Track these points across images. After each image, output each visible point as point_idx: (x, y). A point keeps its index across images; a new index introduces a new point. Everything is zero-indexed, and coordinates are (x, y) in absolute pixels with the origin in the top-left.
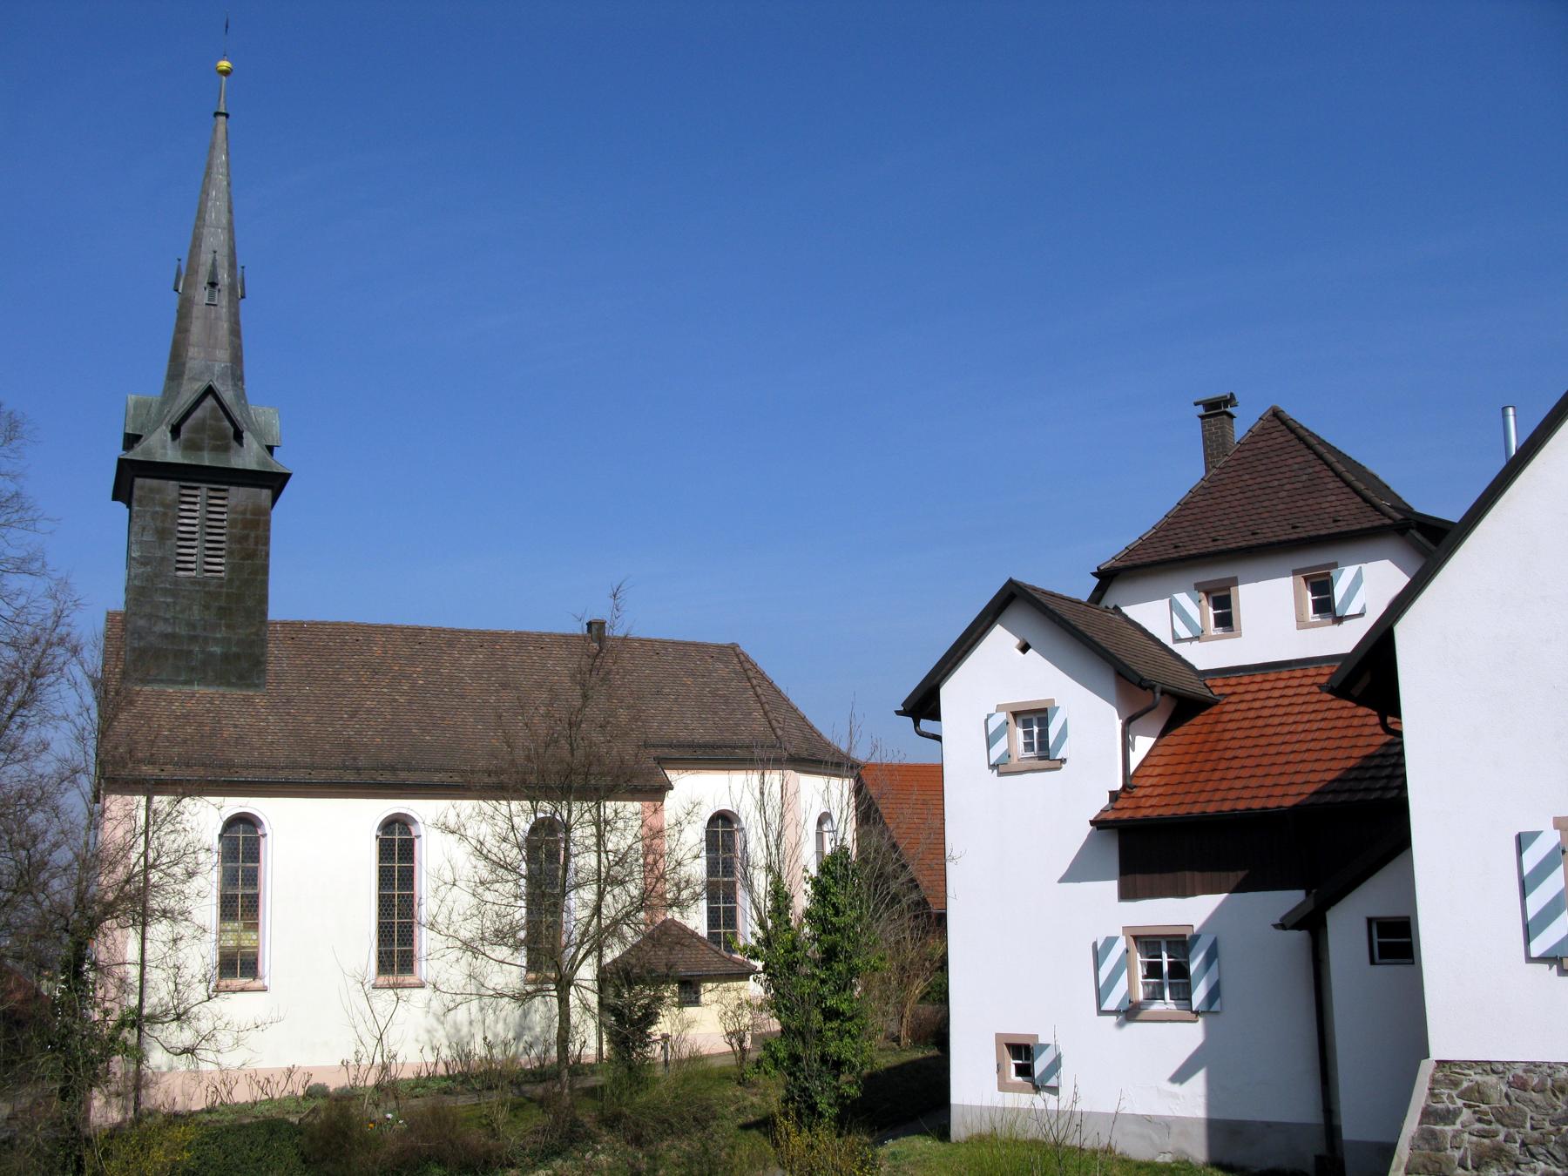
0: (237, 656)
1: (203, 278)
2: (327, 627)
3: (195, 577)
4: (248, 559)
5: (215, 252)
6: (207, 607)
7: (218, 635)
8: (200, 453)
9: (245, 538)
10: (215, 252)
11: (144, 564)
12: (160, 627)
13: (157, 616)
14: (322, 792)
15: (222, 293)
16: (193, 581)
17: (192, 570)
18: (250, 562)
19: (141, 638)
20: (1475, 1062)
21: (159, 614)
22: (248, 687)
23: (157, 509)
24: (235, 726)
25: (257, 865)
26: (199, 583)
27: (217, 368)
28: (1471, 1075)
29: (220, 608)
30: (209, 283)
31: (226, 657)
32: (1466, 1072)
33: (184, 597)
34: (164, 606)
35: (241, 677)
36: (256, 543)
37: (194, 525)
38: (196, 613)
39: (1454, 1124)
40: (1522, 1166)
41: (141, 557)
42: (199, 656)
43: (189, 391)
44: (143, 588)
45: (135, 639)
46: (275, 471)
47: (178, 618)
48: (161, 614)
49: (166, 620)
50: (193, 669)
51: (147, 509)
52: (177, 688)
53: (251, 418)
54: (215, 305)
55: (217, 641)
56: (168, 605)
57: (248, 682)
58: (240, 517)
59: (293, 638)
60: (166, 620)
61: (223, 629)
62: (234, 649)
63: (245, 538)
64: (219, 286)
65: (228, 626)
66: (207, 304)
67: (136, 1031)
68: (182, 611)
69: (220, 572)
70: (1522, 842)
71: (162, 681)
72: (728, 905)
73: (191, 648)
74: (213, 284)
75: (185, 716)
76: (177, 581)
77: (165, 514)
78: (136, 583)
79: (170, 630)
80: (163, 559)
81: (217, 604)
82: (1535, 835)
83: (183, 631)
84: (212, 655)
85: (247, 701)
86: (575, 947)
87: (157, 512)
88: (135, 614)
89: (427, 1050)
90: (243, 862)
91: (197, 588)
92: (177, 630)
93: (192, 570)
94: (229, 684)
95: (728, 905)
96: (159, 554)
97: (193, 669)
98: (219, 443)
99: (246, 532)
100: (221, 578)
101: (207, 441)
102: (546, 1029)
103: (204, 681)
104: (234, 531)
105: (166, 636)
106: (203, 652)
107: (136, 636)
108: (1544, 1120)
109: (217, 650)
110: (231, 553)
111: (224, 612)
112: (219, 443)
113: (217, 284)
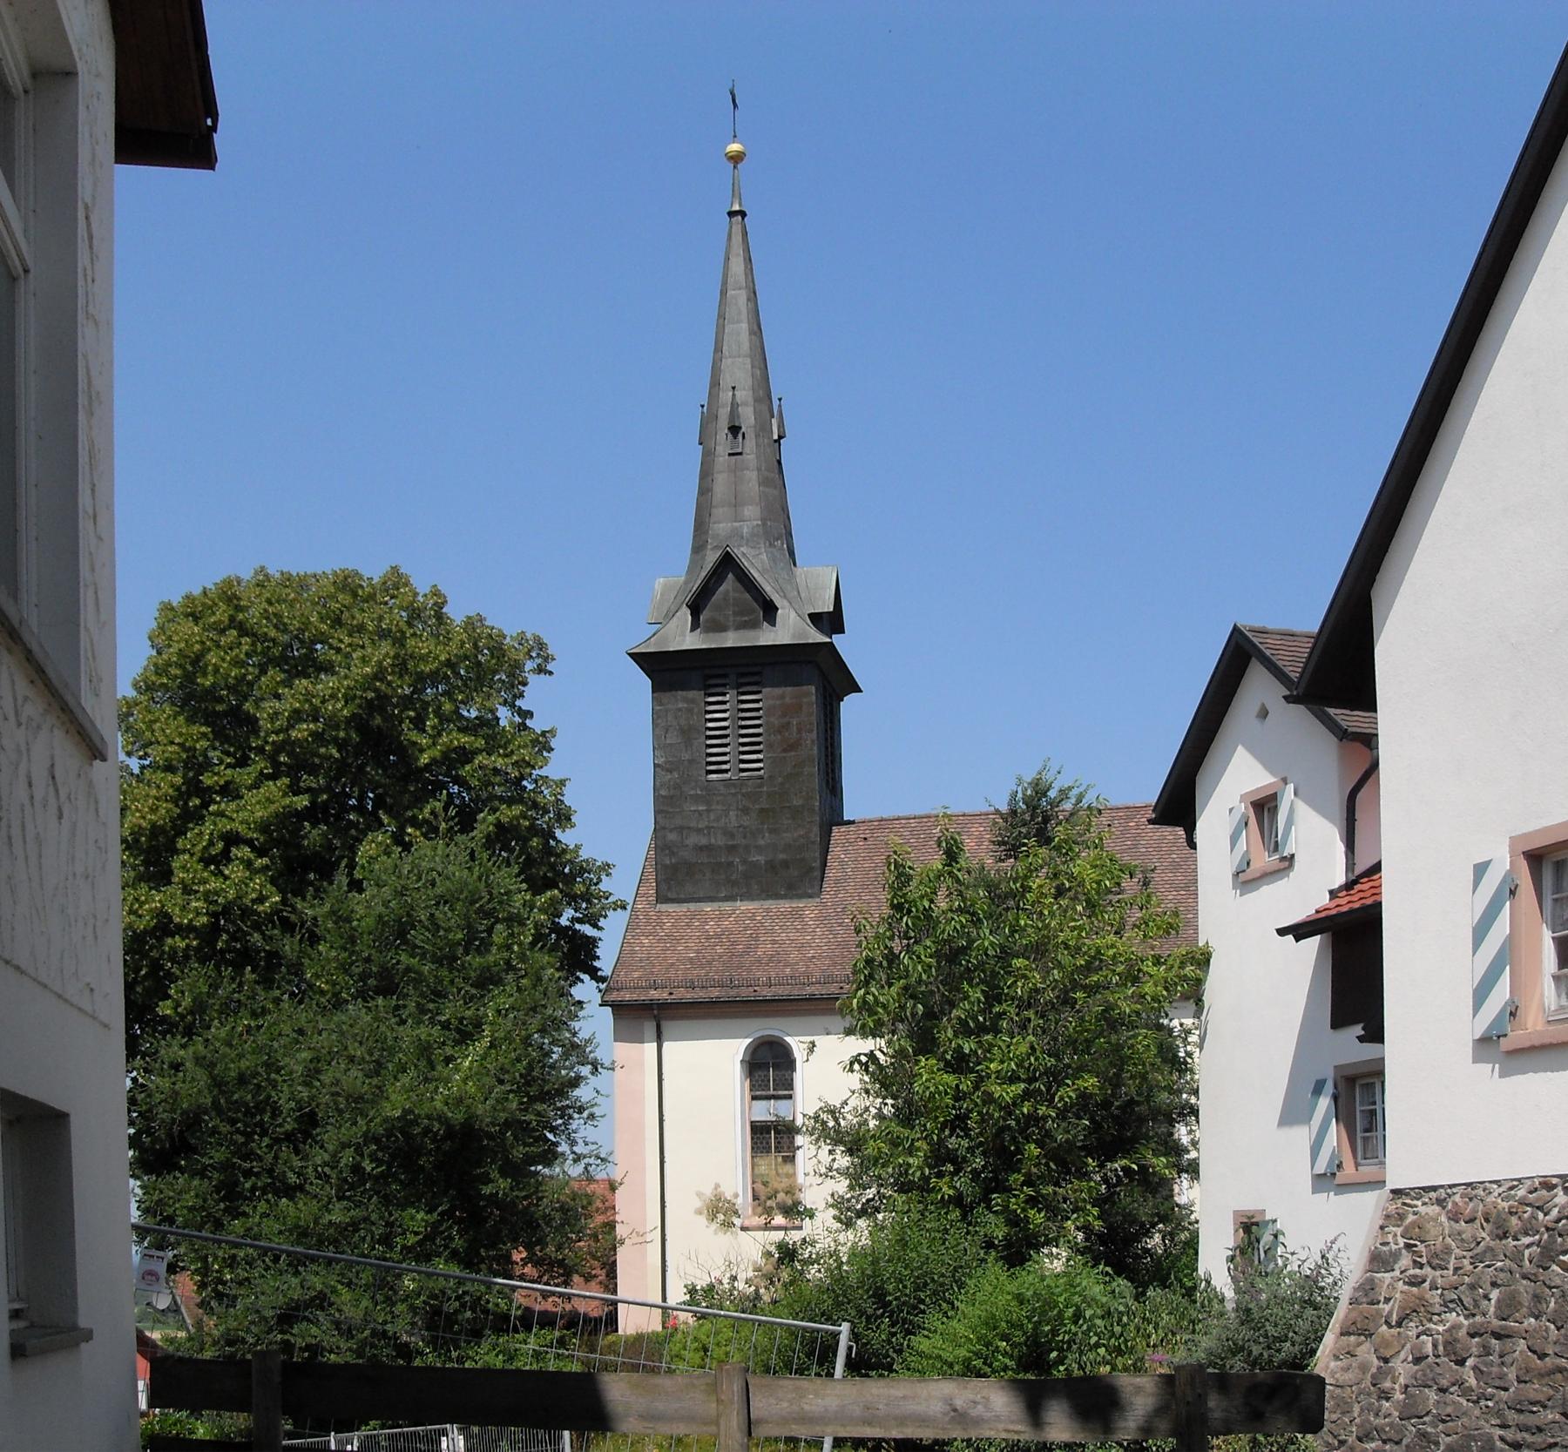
0: (785, 864)
1: (723, 424)
2: (912, 821)
3: (730, 779)
4: (790, 751)
5: (734, 388)
7: (761, 842)
8: (723, 634)
9: (787, 726)
10: (734, 388)
12: (693, 840)
13: (689, 828)
15: (747, 441)
17: (726, 771)
18: (793, 753)
19: (672, 854)
20: (1423, 1188)
21: (692, 825)
22: (800, 897)
23: (680, 705)
24: (774, 942)
25: (791, 1092)
26: (734, 785)
27: (745, 530)
28: (1416, 1206)
29: (762, 810)
30: (729, 429)
31: (772, 866)
32: (1415, 1202)
33: (718, 803)
34: (696, 815)
36: (799, 731)
37: (724, 719)
38: (733, 819)
39: (1393, 1270)
40: (1435, 1318)
41: (666, 763)
42: (740, 868)
43: (712, 558)
44: (672, 797)
45: (666, 855)
46: (811, 641)
47: (713, 827)
48: (693, 824)
49: (699, 831)
51: (670, 706)
52: (716, 905)
54: (740, 454)
55: (760, 849)
56: (700, 813)
57: (800, 892)
58: (778, 702)
59: (865, 839)
60: (699, 831)
61: (767, 835)
62: (782, 856)
63: (786, 726)
64: (743, 430)
65: (771, 831)
66: (730, 455)
68: (718, 819)
69: (758, 769)
70: (1480, 870)
71: (699, 900)
73: (731, 859)
74: (735, 430)
75: (717, 936)
77: (690, 711)
78: (663, 792)
79: (704, 841)
80: (691, 761)
81: (757, 807)
82: (1487, 864)
83: (719, 840)
84: (755, 865)
85: (797, 915)
87: (680, 710)
88: (664, 828)
90: (774, 1090)
91: (733, 791)
92: (713, 841)
93: (726, 771)
94: (777, 896)
96: (686, 756)
98: (746, 618)
99: (786, 720)
100: (761, 778)
101: (731, 619)
103: (748, 896)
104: (772, 719)
105: (701, 849)
107: (667, 852)
108: (1464, 1257)
109: (760, 858)
110: (770, 746)
112: (746, 618)
113: (740, 428)
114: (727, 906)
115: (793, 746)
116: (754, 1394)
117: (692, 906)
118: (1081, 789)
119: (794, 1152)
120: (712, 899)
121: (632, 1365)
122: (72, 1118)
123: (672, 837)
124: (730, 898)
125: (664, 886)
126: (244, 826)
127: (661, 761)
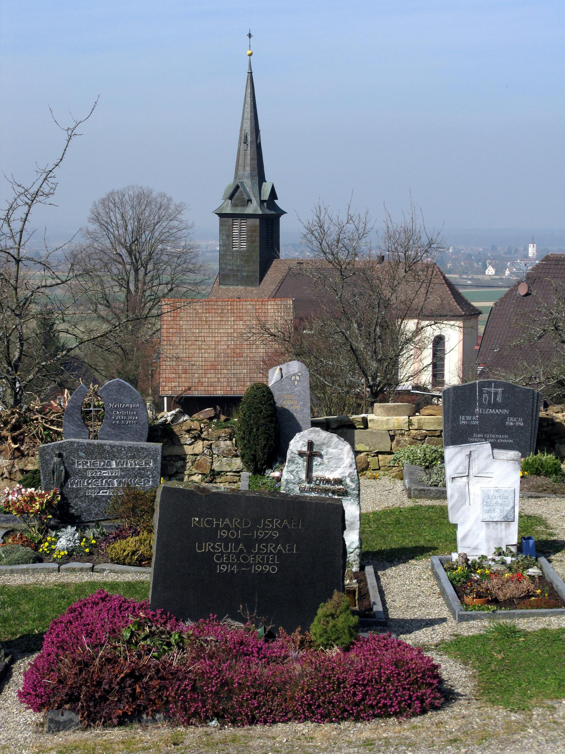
0: (251, 276)
6: (241, 260)
9: (252, 236)
11: (224, 247)
12: (229, 267)
14: (552, 613)
16: (237, 251)
31: (247, 277)
35: (252, 283)
50: (238, 281)
53: (446, 320)
62: (250, 274)
67: (213, 468)
71: (230, 285)
72: (117, 443)
76: (233, 252)
79: (231, 268)
83: (235, 268)
84: (243, 276)
86: (147, 281)
89: (16, 187)
95: (117, 443)
97: (238, 281)
102: (51, 570)
105: (230, 270)
106: (241, 275)
109: (245, 274)
111: (246, 261)
114: (236, 287)
115: (253, 242)
116: (21, 269)
117: (228, 287)
118: (423, 227)
119: (433, 361)
120: (233, 285)
121: (411, 495)
122: (446, 339)
123: (224, 266)
124: (237, 285)
125: (221, 280)
126: (251, 665)
127: (221, 243)
